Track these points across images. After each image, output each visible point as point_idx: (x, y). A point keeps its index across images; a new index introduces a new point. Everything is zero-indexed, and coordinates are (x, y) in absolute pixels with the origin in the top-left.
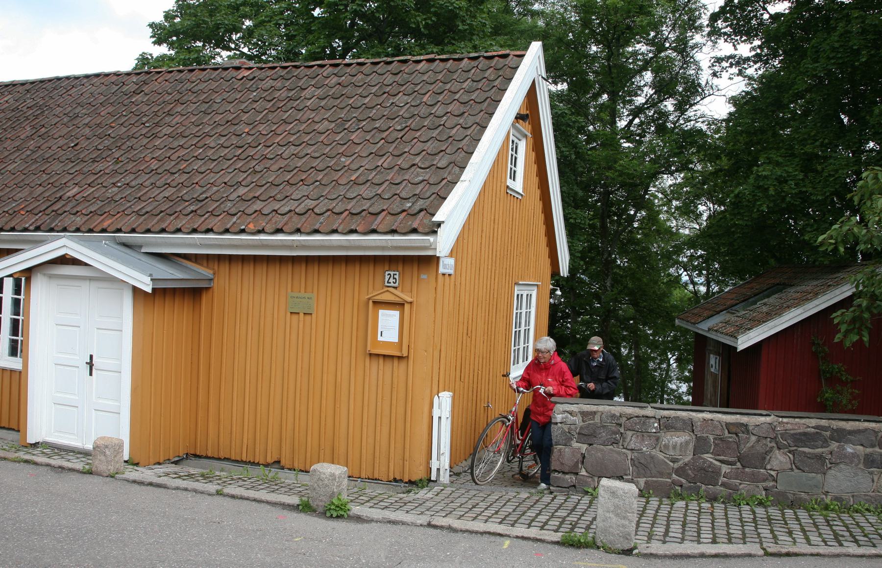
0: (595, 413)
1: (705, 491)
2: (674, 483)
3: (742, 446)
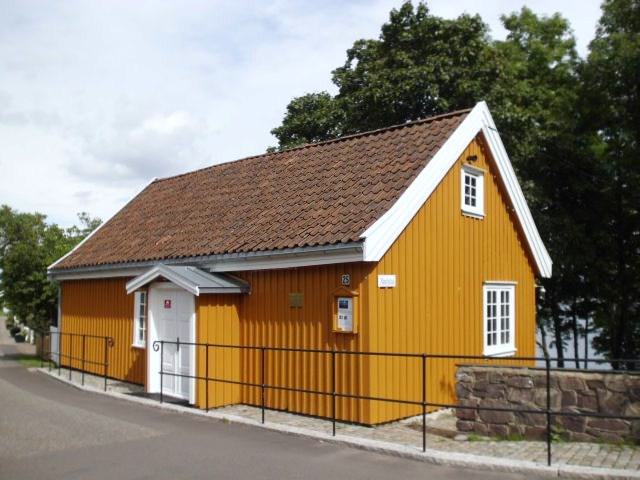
0: (485, 373)
3: (600, 400)
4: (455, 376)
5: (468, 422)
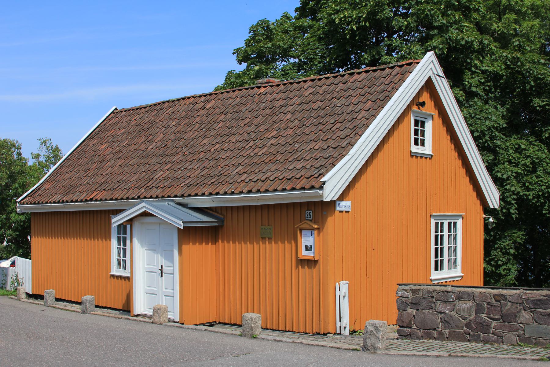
1: (483, 337)
2: (465, 332)
3: (503, 309)
4: (397, 293)
5: (406, 329)
